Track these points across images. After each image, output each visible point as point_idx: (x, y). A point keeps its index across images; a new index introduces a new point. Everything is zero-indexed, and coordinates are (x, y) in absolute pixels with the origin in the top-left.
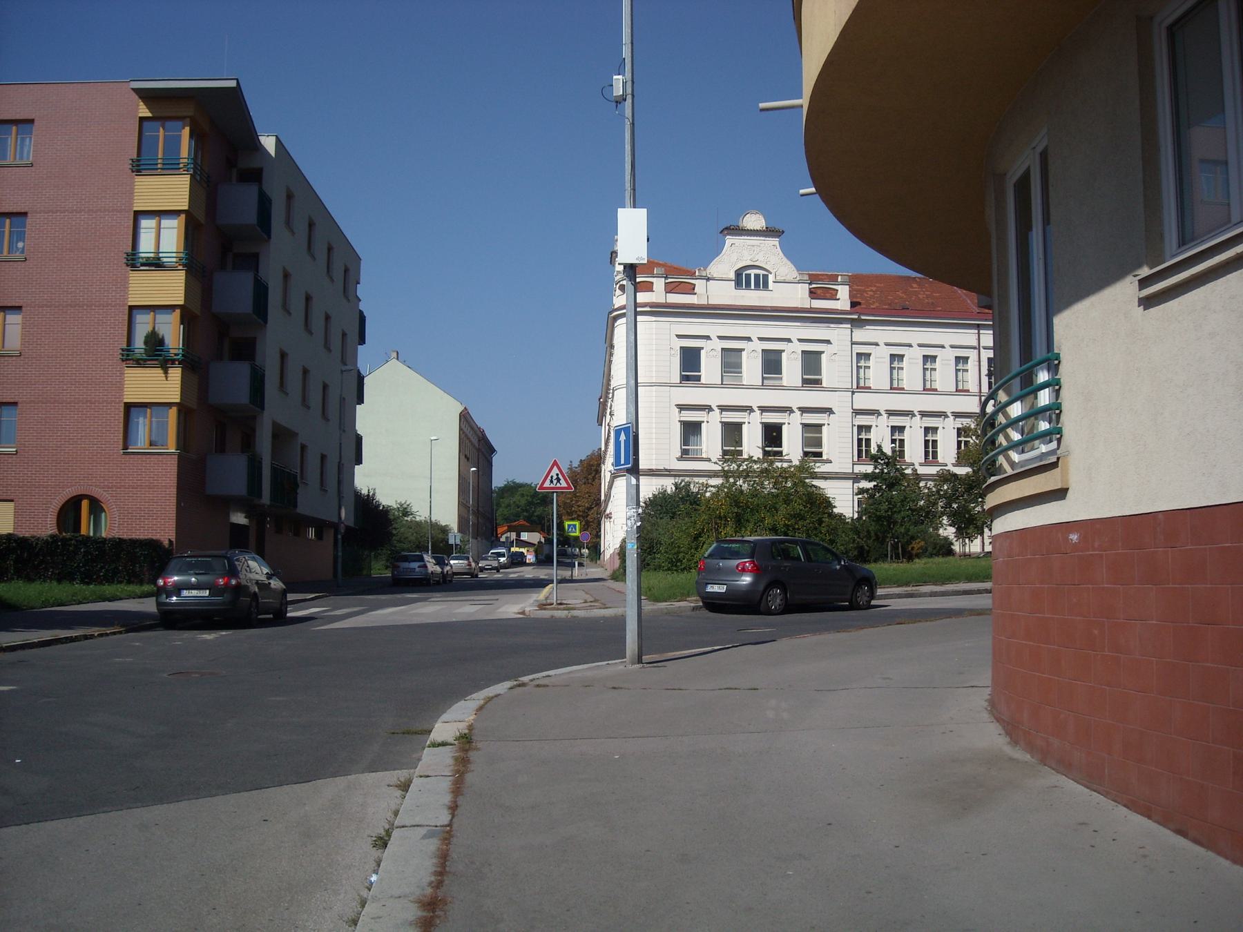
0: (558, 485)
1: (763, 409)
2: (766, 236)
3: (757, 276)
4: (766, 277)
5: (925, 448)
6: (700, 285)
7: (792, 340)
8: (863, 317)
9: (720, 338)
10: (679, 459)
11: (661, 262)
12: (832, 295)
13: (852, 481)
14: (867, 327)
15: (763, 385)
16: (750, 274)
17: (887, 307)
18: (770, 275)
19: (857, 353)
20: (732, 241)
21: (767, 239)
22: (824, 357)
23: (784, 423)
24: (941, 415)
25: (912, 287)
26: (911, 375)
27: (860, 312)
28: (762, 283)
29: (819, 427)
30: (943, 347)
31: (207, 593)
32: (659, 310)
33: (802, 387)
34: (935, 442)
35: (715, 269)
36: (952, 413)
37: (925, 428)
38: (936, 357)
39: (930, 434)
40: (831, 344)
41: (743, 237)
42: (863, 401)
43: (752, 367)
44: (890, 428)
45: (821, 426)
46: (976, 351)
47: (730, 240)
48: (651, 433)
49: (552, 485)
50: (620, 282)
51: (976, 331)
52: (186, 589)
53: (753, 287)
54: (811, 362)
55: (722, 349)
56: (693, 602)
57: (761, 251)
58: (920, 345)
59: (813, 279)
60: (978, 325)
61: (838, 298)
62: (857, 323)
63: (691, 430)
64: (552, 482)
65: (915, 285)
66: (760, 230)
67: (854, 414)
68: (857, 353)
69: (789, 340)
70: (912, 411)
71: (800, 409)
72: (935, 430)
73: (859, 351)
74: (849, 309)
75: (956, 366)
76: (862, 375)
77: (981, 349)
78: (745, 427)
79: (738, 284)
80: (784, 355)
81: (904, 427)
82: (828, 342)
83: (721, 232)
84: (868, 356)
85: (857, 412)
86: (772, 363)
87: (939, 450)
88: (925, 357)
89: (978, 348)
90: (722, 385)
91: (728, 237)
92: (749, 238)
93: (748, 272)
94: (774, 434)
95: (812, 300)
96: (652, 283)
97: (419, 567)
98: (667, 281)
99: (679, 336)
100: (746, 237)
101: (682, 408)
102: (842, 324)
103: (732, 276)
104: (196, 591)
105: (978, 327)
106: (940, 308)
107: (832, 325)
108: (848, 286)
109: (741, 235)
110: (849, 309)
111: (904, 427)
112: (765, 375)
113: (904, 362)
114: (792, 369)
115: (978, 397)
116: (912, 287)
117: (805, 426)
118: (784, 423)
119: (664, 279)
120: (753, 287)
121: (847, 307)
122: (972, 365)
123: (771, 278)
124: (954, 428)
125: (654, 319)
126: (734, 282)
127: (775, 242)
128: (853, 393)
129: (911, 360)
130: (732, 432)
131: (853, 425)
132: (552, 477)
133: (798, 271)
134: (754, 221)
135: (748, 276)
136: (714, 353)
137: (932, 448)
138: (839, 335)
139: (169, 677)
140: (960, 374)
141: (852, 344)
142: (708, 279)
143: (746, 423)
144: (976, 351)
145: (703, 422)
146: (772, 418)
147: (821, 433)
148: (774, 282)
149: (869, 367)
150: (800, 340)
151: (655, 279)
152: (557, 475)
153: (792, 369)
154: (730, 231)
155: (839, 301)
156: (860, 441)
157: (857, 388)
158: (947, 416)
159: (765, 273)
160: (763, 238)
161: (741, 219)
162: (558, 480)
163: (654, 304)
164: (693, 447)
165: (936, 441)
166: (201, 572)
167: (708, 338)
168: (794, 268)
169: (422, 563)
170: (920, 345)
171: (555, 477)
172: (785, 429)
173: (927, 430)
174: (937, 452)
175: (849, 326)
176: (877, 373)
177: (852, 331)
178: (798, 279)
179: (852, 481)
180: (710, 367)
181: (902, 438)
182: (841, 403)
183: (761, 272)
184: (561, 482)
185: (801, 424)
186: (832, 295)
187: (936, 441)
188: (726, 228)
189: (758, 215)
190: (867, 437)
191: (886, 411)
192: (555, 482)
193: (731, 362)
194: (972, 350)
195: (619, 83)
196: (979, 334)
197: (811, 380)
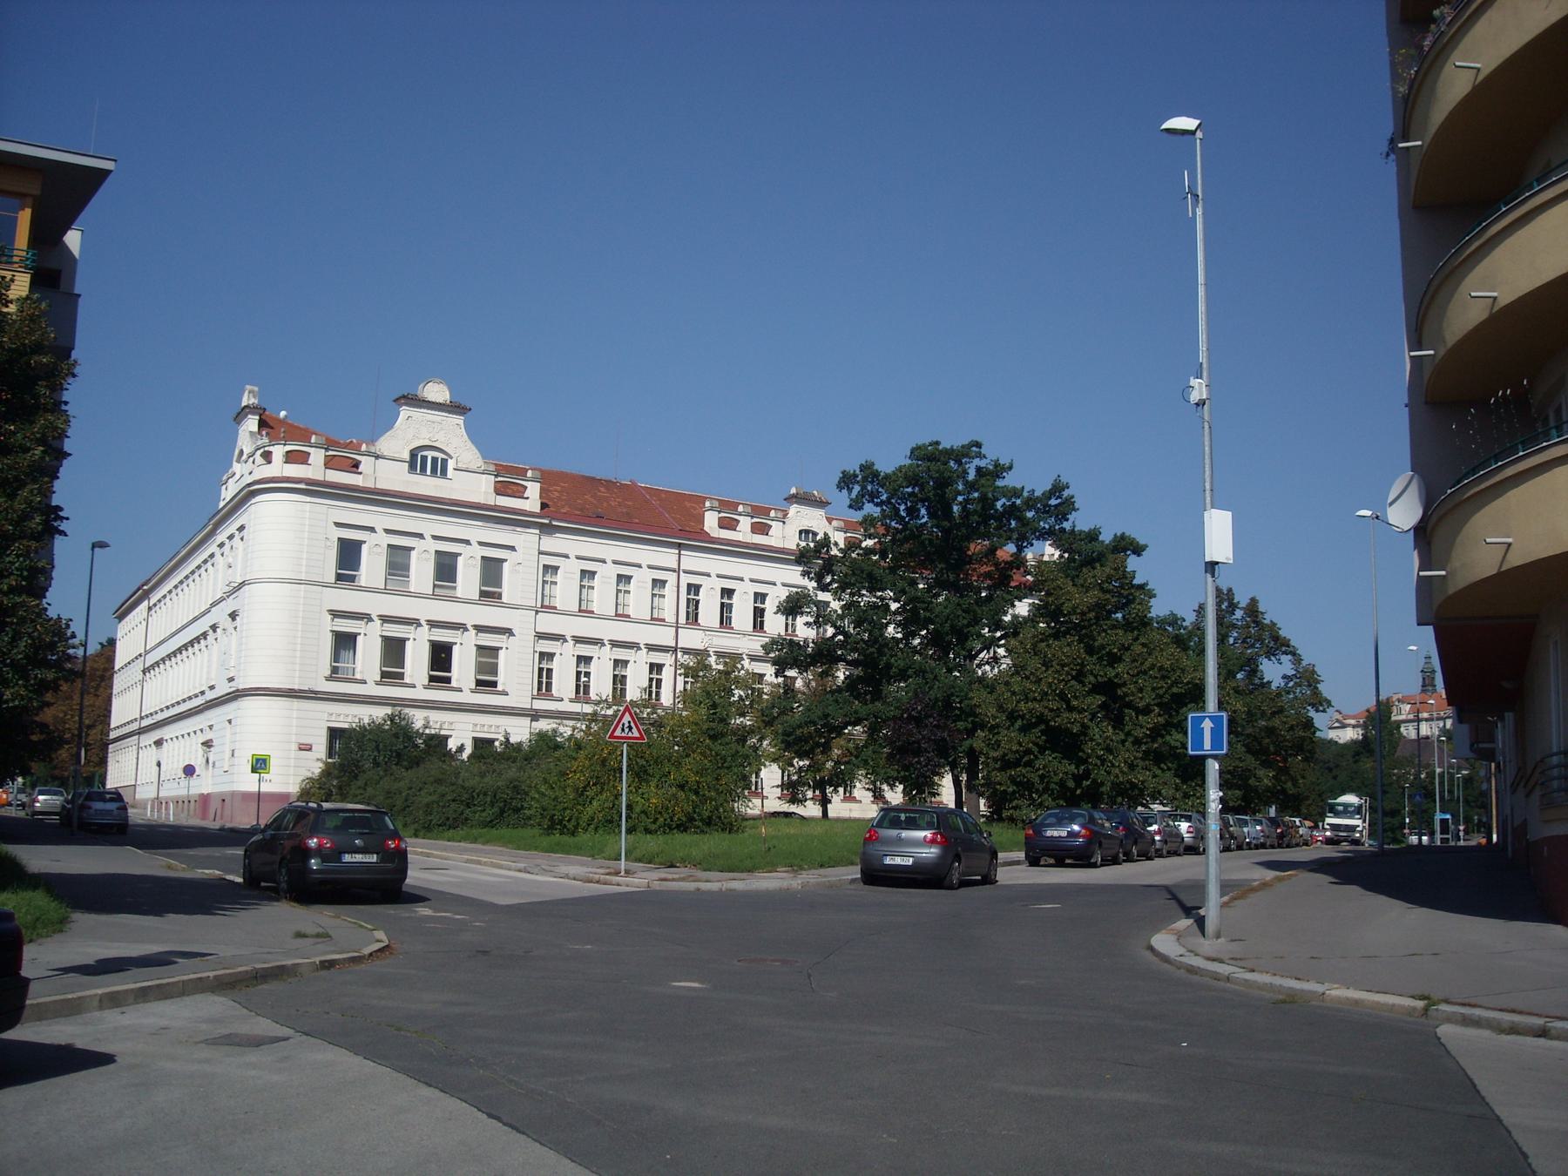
0: (630, 735)
1: (433, 624)
2: (449, 412)
3: (435, 460)
4: (444, 462)
5: (577, 681)
6: (366, 463)
7: (471, 542)
8: (554, 523)
9: (387, 531)
10: (327, 679)
11: (301, 426)
12: (519, 492)
13: (530, 718)
14: (557, 535)
15: (433, 595)
16: (427, 457)
17: (578, 513)
18: (449, 461)
19: (544, 566)
20: (409, 413)
21: (451, 415)
22: (505, 565)
23: (409, 639)
24: (597, 642)
25: (600, 491)
26: (602, 595)
27: (549, 519)
28: (439, 469)
29: (494, 651)
30: (604, 561)
31: (374, 858)
32: (315, 489)
33: (480, 600)
34: (550, 671)
35: (385, 445)
36: (646, 644)
37: (615, 660)
38: (630, 577)
39: (545, 661)
40: (376, 532)
41: (422, 410)
42: (548, 623)
43: (421, 571)
44: (576, 657)
45: (497, 649)
46: (675, 574)
47: (405, 412)
48: (296, 644)
49: (623, 735)
50: (265, 447)
51: (677, 551)
52: (348, 853)
53: (429, 472)
54: (492, 570)
55: (482, 557)
56: (855, 872)
57: (442, 429)
58: (615, 562)
59: (499, 470)
60: (680, 544)
61: (525, 496)
62: (547, 529)
63: (344, 642)
64: (623, 730)
65: (602, 489)
66: (444, 404)
67: (537, 638)
68: (544, 566)
69: (467, 542)
70: (418, 620)
71: (381, 617)
72: (626, 663)
73: (546, 563)
74: (539, 511)
75: (581, 581)
76: (547, 592)
77: (681, 572)
78: (409, 645)
79: (412, 467)
80: (460, 560)
81: (592, 658)
82: (512, 548)
83: (396, 400)
84: (556, 569)
85: (541, 636)
86: (446, 569)
87: (628, 687)
88: (654, 581)
89: (677, 571)
90: (385, 591)
91: (404, 407)
92: (429, 411)
93: (425, 453)
94: (443, 655)
95: (498, 497)
96: (309, 454)
97: (118, 809)
98: (327, 454)
99: (338, 525)
100: (425, 411)
101: (336, 614)
102: (529, 528)
103: (406, 456)
104: (361, 856)
105: (679, 546)
106: (637, 521)
107: (518, 529)
108: (539, 484)
109: (421, 407)
110: (539, 511)
111: (592, 658)
112: (436, 583)
113: (596, 580)
114: (468, 578)
115: (674, 629)
116: (600, 491)
117: (480, 648)
118: (409, 639)
119: (323, 450)
120: (429, 472)
121: (537, 509)
122: (669, 590)
123: (451, 464)
124: (574, 655)
125: (308, 499)
126: (407, 464)
127: (458, 420)
128: (537, 612)
129: (639, 584)
130: (394, 650)
131: (535, 652)
132: (623, 725)
133: (484, 458)
134: (436, 392)
135: (424, 459)
136: (713, 592)
137: (547, 678)
138: (526, 541)
139: (740, 964)
140: (585, 591)
141: (539, 553)
142: (377, 457)
143: (411, 640)
144: (675, 574)
145: (360, 634)
146: (443, 636)
147: (497, 658)
148: (455, 469)
149: (593, 588)
150: (481, 544)
151: (313, 449)
152: (629, 722)
153: (468, 578)
154: (409, 401)
155: (528, 501)
156: (541, 670)
157: (542, 607)
158: (419, 625)
159: (444, 457)
160: (446, 414)
161: (422, 385)
162: (630, 728)
163: (310, 481)
164: (343, 665)
165: (552, 670)
166: (365, 831)
167: (372, 530)
168: (478, 455)
169: (122, 804)
170: (615, 562)
171: (627, 725)
172: (456, 650)
173: (617, 662)
174: (551, 683)
175: (537, 531)
176: (565, 591)
177: (540, 538)
178: (483, 468)
179: (530, 718)
180: (372, 566)
181: (551, 667)
182: (523, 623)
183: (440, 456)
184: (633, 730)
185: (476, 645)
186: (519, 492)
187: (552, 670)
188: (404, 397)
189: (442, 385)
190: (549, 667)
191: (573, 637)
192: (627, 730)
193: (398, 561)
194: (671, 573)
195: (1199, 389)
196: (680, 554)
197: (490, 595)
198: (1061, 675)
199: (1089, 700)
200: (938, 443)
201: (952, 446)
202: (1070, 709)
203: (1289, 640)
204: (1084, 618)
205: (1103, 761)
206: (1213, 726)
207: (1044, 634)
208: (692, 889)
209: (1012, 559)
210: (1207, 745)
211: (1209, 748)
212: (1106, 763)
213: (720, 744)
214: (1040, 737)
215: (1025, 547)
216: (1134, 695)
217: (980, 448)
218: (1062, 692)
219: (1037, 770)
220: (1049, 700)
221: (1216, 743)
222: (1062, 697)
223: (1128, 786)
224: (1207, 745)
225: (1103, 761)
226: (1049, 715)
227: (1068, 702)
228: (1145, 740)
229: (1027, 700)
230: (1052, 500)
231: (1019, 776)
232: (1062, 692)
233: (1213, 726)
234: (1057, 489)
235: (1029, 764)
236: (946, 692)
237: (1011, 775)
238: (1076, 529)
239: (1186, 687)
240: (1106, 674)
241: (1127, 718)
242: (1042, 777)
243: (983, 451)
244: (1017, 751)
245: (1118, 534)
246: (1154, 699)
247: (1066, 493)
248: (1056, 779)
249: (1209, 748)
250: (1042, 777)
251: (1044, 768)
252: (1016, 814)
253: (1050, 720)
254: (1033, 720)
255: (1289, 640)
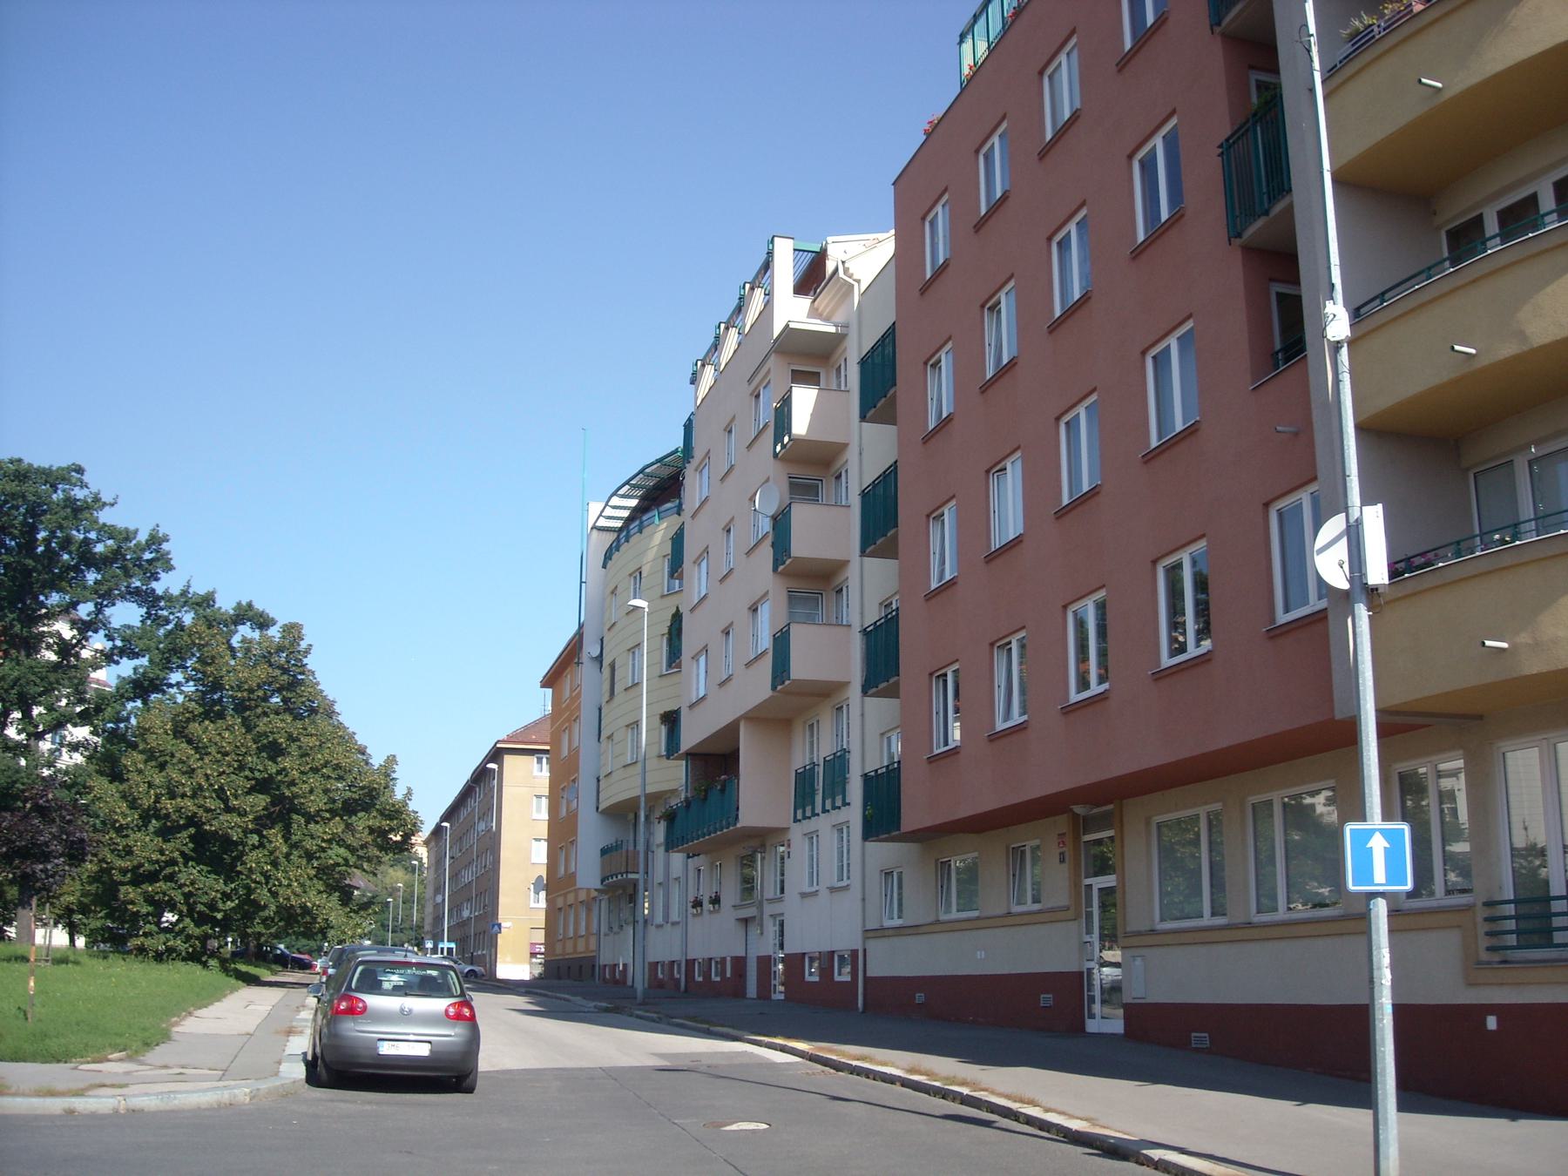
198: (221, 766)
199: (251, 799)
200: (20, 461)
201: (51, 466)
202: (229, 810)
203: (366, 747)
204: (251, 696)
205: (267, 878)
206: (1388, 846)
207: (192, 712)
208: (59, 1112)
209: (89, 618)
210: (1380, 875)
211: (1384, 881)
212: (271, 881)
213: (744, 848)
214: (186, 845)
215: (106, 606)
216: (305, 797)
217: (82, 474)
218: (221, 788)
219: (181, 886)
220: (205, 798)
221: (1393, 873)
222: (220, 793)
223: (299, 911)
224: (1380, 875)
225: (267, 878)
226: (204, 816)
227: (225, 801)
228: (318, 855)
229: (172, 796)
230: (147, 553)
231: (157, 893)
232: (221, 788)
233: (1388, 846)
234: (155, 540)
235: (170, 878)
236: (10, 777)
237: (147, 892)
238: (191, 591)
239: (361, 792)
240: (266, 770)
241: (295, 826)
242: (187, 896)
243: (86, 478)
244: (157, 862)
245: (244, 603)
246: (325, 804)
247: (165, 546)
248: (204, 899)
249: (1384, 881)
250: (187, 896)
251: (192, 883)
252: (148, 942)
253: (205, 823)
254: (181, 822)
255: (366, 747)
